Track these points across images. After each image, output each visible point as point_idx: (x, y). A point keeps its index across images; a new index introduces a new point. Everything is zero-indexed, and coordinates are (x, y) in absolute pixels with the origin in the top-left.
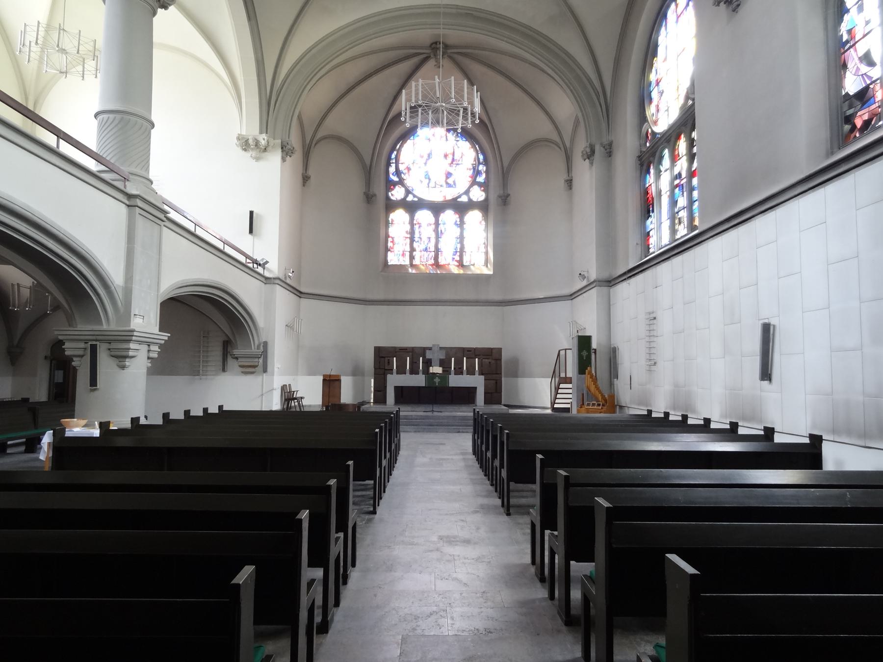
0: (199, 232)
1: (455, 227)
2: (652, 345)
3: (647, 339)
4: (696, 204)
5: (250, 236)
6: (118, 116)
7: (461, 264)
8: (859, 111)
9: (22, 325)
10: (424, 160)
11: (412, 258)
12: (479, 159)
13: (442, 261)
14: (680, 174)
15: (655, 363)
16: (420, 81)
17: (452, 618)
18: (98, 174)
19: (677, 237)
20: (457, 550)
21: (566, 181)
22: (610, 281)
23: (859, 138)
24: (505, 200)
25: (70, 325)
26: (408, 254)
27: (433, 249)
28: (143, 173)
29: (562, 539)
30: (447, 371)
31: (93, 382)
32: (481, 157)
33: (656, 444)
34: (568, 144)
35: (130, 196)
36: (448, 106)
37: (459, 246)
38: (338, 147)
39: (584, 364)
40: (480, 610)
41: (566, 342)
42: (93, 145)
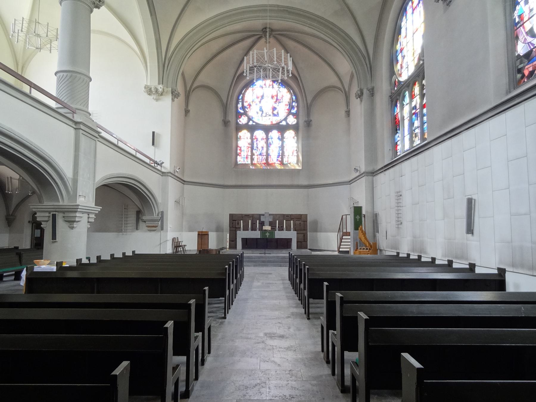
0: (121, 145)
1: (278, 141)
2: (400, 212)
3: (396, 208)
4: (426, 125)
5: (153, 147)
6: (69, 74)
7: (282, 163)
8: (527, 65)
9: (15, 202)
10: (259, 99)
11: (252, 159)
12: (292, 99)
13: (270, 161)
14: (415, 106)
15: (401, 223)
16: (255, 51)
17: (269, 388)
18: (56, 110)
19: (415, 145)
20: (275, 342)
21: (346, 112)
22: (373, 173)
23: (527, 82)
24: (308, 124)
25: (40, 202)
26: (249, 157)
27: (265, 154)
28: (84, 108)
29: (339, 336)
30: (273, 229)
31: (54, 237)
32: (294, 98)
33: (400, 274)
34: (347, 89)
35: (76, 123)
36: (272, 66)
37: (281, 152)
38: (206, 94)
39: (357, 224)
40: (287, 383)
41: (347, 210)
42: (54, 93)
